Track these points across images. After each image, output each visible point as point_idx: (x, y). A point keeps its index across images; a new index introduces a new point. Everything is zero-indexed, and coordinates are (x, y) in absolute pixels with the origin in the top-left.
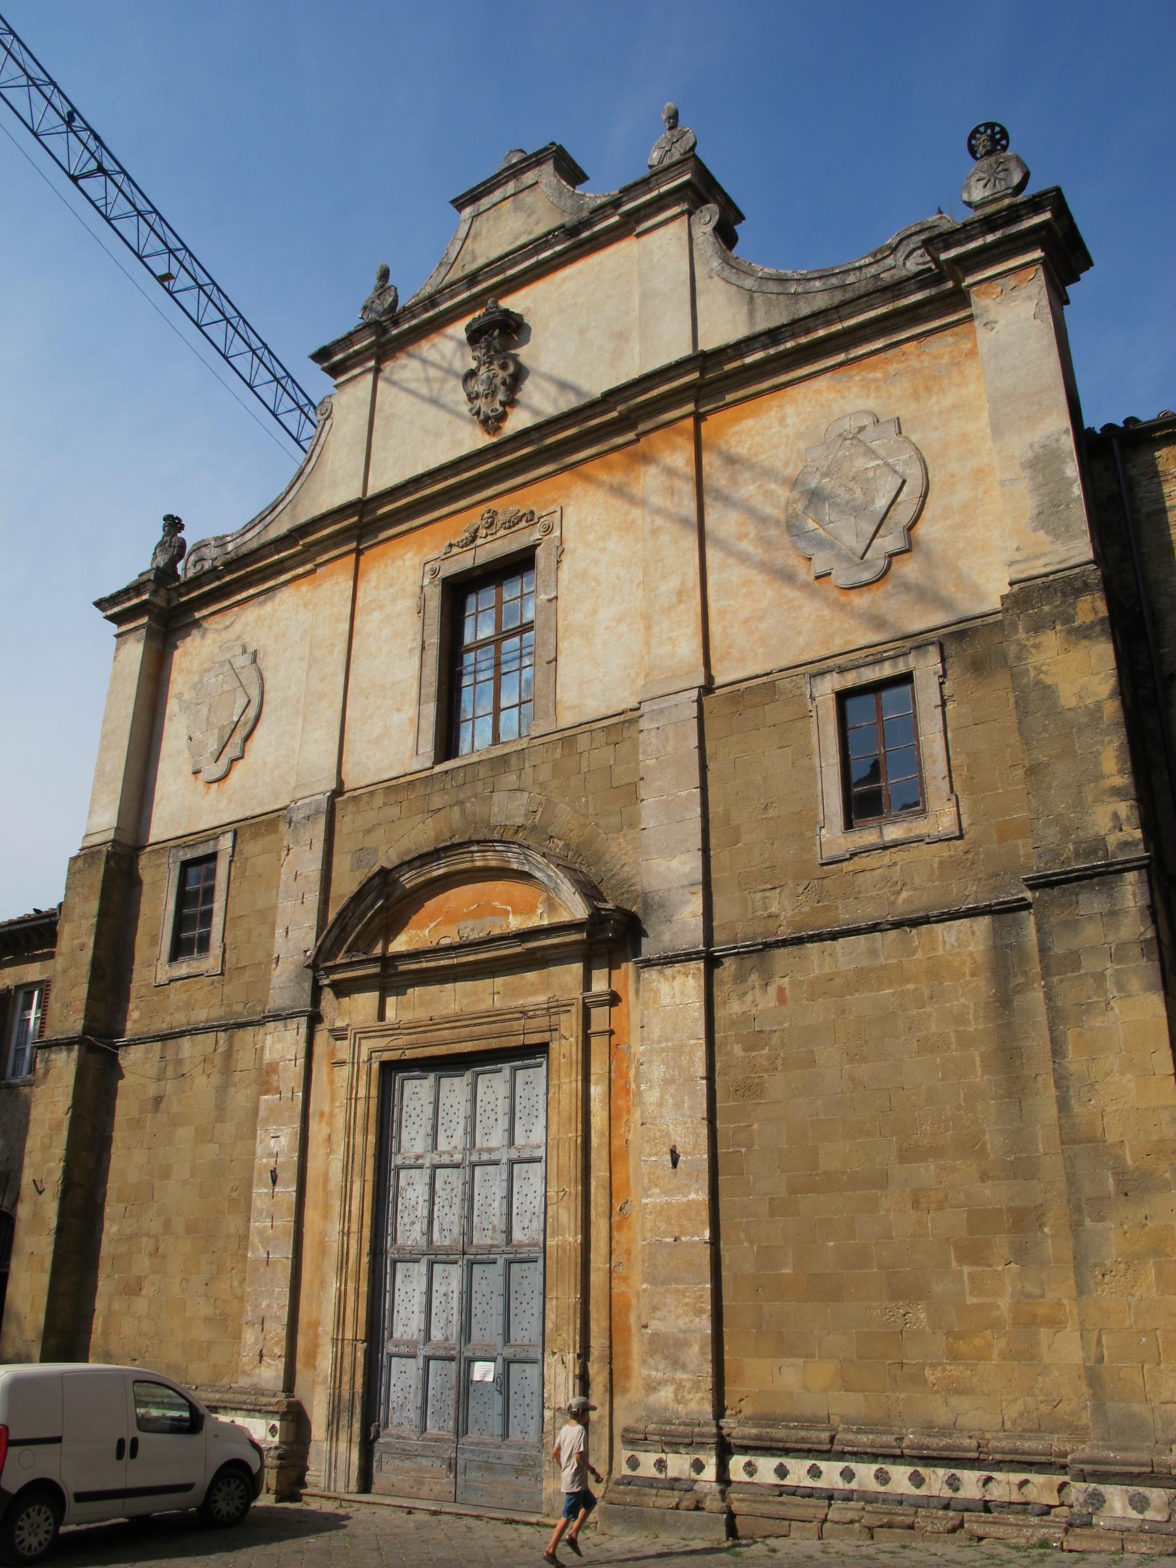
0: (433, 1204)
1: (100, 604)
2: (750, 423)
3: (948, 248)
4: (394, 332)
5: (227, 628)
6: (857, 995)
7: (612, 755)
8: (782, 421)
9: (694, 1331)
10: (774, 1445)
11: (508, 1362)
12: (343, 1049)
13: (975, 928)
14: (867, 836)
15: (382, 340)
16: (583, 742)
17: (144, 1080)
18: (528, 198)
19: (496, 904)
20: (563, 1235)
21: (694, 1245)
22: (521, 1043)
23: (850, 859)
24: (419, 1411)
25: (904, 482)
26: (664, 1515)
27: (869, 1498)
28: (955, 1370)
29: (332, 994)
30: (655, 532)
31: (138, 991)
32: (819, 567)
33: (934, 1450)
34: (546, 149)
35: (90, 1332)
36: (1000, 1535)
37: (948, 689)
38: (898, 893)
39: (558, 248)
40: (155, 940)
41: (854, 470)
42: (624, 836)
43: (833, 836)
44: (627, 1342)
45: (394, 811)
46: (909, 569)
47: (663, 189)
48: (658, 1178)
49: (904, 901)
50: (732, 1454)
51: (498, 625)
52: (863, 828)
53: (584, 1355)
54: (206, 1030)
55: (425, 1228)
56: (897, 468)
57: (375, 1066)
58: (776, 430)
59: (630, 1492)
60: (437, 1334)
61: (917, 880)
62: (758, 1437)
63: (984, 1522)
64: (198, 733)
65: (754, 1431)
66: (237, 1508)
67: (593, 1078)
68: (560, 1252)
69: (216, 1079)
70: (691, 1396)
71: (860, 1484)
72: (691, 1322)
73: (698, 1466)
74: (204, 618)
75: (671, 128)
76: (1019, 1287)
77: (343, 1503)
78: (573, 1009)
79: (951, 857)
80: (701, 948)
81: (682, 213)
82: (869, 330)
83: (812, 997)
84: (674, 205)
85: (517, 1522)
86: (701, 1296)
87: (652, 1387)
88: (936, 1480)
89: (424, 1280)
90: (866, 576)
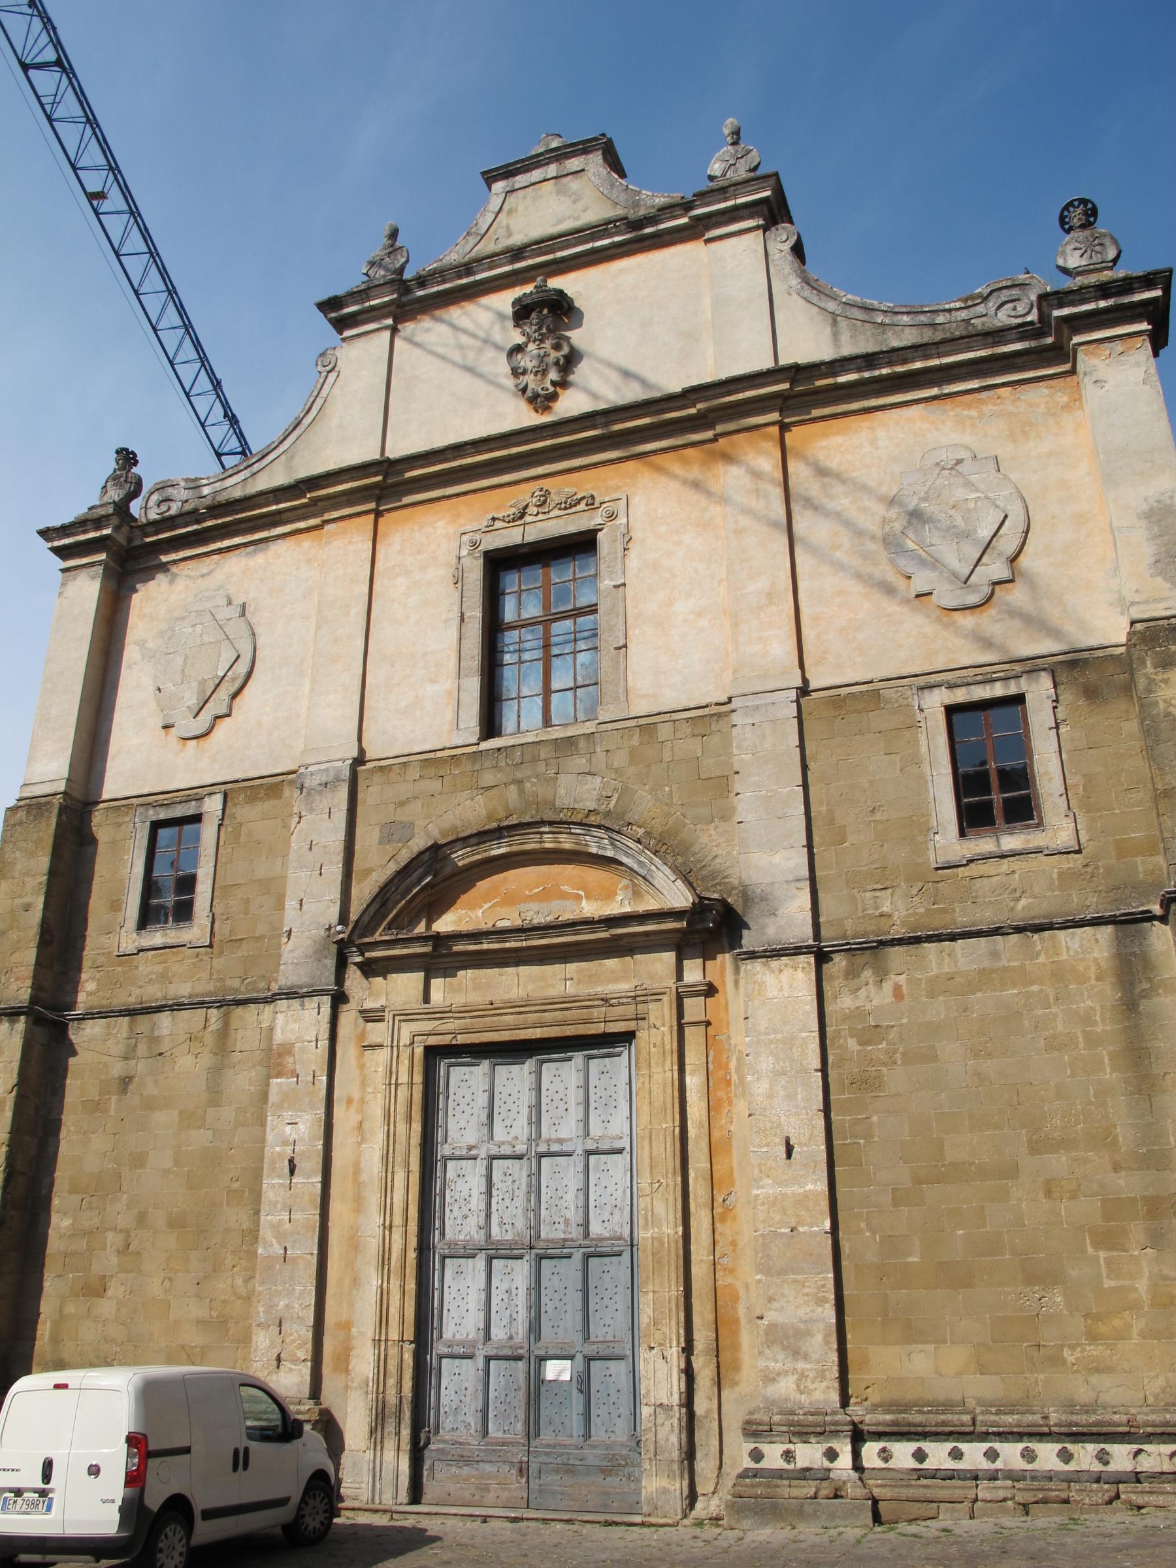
0: (491, 1196)
1: (45, 534)
2: (837, 440)
3: (1061, 306)
4: (421, 293)
5: (203, 576)
6: (979, 994)
7: (699, 747)
8: (874, 442)
9: (816, 1321)
10: (913, 1429)
11: (589, 1360)
12: (378, 1032)
13: (1099, 936)
14: (984, 844)
15: (404, 299)
16: (665, 732)
17: (105, 1059)
18: (573, 184)
19: (566, 888)
20: (660, 1227)
21: (814, 1235)
22: (601, 1031)
23: (966, 865)
24: (479, 1414)
25: (1006, 517)
26: (802, 1505)
27: (1014, 1476)
28: (1095, 1350)
29: (359, 973)
30: (739, 532)
31: (94, 961)
32: (920, 582)
33: (1083, 1426)
34: (595, 139)
35: (34, 1339)
36: (1160, 1503)
37: (1061, 713)
38: (1018, 900)
39: (617, 239)
40: (116, 906)
41: (954, 499)
42: (716, 828)
43: (947, 841)
44: (735, 1333)
45: (434, 785)
46: (1016, 595)
47: (740, 201)
48: (770, 1169)
49: (1024, 908)
50: (865, 1441)
51: (546, 606)
52: (978, 835)
53: (688, 1349)
54: (192, 1006)
55: (482, 1222)
56: (998, 503)
57: (419, 1051)
58: (876, 449)
59: (759, 1485)
60: (498, 1333)
61: (1036, 889)
62: (895, 1423)
63: (1142, 1492)
64: (170, 685)
65: (889, 1417)
66: (322, 1523)
67: (688, 1068)
68: (656, 1245)
69: (206, 1059)
70: (815, 1386)
71: (1005, 1463)
72: (813, 1311)
73: (832, 1455)
74: (174, 562)
75: (733, 144)
76: (1156, 1270)
77: (395, 1516)
78: (665, 998)
79: (1069, 869)
80: (811, 942)
81: (757, 228)
82: (964, 370)
83: (931, 995)
84: (748, 219)
85: (617, 1524)
86: (823, 1286)
87: (770, 1378)
88: (1085, 1456)
89: (483, 1275)
90: (973, 599)
